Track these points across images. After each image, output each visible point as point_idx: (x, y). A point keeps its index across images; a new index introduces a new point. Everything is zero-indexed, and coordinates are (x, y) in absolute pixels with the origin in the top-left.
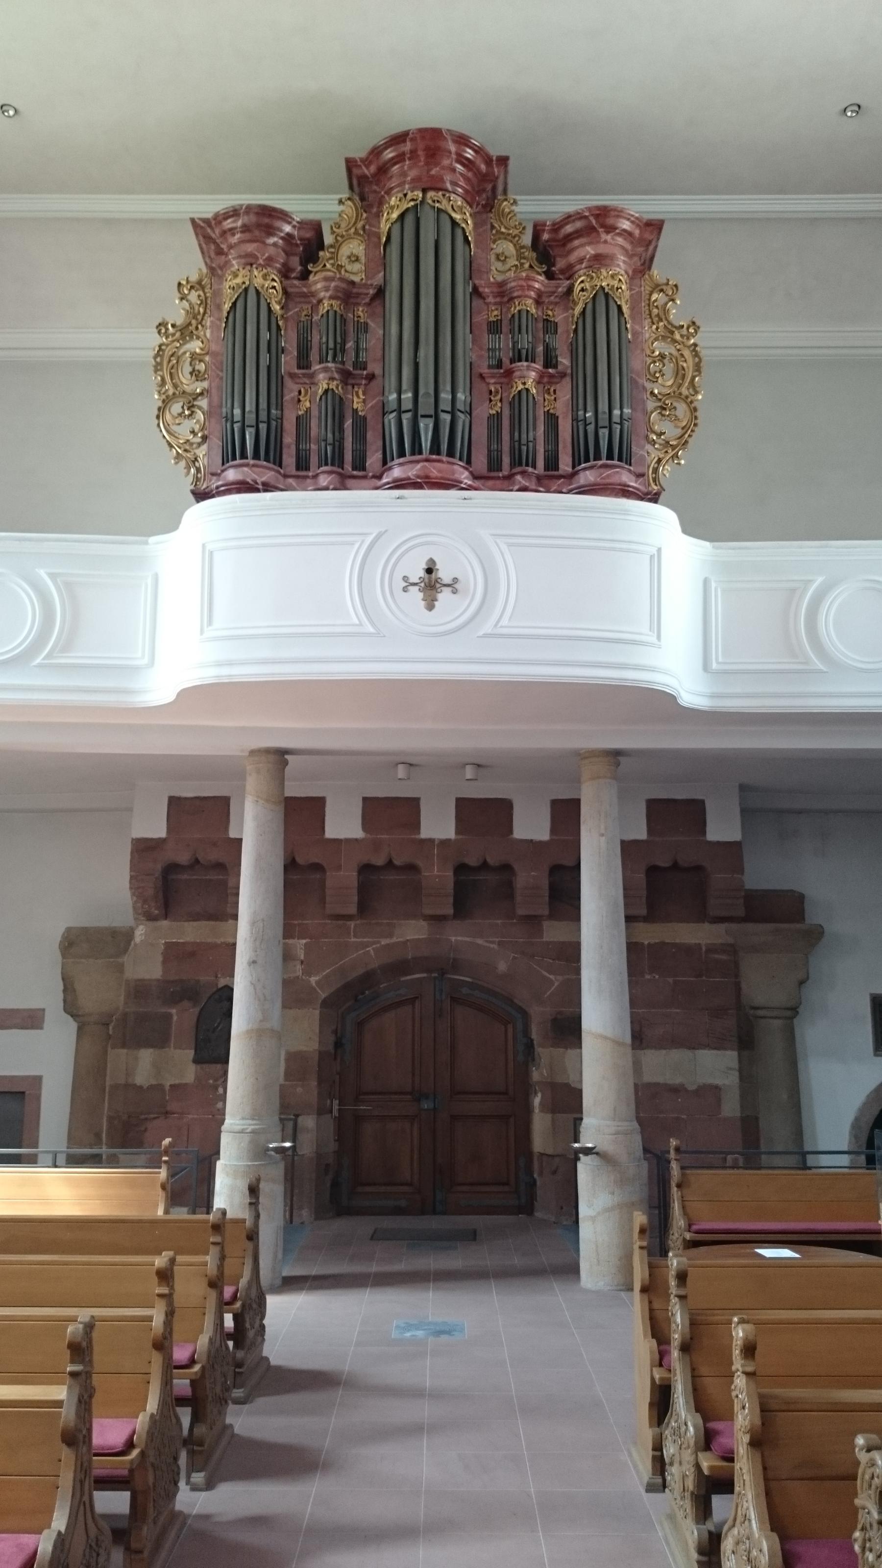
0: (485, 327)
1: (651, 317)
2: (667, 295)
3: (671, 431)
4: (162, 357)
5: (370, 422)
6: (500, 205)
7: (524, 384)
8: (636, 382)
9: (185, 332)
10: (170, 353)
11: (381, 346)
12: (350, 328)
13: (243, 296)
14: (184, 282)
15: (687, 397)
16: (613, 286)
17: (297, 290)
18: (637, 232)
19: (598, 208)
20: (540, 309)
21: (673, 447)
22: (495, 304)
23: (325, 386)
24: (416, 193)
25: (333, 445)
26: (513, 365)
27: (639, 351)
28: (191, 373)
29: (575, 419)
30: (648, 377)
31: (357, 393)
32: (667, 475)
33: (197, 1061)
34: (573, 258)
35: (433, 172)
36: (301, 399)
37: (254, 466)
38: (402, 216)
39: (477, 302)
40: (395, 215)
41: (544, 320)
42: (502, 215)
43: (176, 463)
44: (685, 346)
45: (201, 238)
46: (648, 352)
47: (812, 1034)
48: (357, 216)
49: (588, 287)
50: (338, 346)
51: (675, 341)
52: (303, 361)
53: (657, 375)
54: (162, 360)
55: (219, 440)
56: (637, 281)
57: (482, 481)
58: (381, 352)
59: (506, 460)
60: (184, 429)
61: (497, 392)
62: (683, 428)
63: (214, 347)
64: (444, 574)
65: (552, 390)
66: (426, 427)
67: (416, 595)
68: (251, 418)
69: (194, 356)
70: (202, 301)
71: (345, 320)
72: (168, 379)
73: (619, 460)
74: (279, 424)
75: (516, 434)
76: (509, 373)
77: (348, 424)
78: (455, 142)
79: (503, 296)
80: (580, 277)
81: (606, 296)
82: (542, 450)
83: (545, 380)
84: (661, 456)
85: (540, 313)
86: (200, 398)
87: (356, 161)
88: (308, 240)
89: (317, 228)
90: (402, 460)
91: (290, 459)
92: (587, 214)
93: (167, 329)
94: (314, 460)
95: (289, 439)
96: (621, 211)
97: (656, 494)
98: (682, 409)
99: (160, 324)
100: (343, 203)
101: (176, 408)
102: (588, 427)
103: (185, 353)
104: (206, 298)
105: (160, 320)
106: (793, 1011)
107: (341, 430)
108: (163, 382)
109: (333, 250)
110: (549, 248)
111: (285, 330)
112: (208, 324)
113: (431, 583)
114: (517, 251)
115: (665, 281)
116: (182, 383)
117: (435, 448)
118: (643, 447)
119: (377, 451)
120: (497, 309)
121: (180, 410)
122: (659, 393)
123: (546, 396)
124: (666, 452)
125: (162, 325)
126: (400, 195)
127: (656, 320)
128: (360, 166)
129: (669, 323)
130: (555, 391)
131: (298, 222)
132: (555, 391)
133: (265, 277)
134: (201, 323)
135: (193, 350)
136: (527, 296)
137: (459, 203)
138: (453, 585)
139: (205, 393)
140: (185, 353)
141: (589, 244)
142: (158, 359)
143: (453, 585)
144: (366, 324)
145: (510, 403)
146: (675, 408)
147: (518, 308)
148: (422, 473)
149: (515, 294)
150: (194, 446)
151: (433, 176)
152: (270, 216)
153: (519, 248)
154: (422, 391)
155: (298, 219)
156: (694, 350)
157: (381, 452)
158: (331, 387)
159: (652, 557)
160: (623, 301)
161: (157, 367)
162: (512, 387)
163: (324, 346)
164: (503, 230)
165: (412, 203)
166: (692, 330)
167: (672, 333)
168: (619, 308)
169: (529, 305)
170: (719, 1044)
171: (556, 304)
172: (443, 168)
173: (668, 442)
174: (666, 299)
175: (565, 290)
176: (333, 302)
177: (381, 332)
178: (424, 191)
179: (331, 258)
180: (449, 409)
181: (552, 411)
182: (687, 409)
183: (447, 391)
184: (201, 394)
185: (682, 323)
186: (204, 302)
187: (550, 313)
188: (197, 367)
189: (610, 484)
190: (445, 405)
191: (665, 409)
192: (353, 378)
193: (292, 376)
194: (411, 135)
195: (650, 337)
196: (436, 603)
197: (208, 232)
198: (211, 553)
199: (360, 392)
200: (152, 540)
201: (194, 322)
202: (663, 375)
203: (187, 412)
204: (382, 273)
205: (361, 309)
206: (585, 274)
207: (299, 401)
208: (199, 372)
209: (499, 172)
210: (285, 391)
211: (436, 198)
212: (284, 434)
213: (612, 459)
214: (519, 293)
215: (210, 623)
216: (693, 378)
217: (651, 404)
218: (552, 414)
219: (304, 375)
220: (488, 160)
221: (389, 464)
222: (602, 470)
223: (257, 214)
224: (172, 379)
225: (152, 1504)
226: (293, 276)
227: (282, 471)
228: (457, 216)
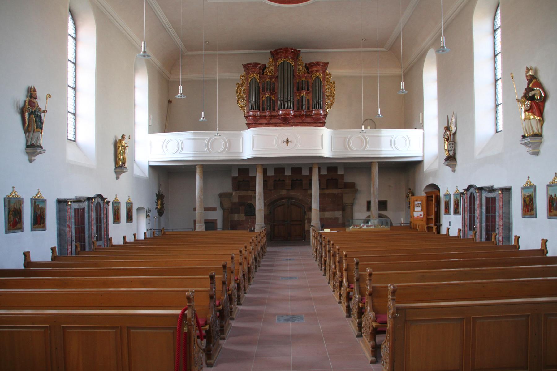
33: (246, 216)
34: (313, 69)
47: (356, 208)
52: (263, 91)
64: (289, 140)
69: (244, 90)
91: (261, 109)
95: (261, 105)
98: (331, 98)
101: (241, 100)
106: (352, 205)
110: (309, 67)
113: (287, 141)
117: (287, 107)
125: (237, 84)
153: (302, 67)
161: (237, 92)
170: (338, 210)
190: (289, 99)
225: (362, 72)
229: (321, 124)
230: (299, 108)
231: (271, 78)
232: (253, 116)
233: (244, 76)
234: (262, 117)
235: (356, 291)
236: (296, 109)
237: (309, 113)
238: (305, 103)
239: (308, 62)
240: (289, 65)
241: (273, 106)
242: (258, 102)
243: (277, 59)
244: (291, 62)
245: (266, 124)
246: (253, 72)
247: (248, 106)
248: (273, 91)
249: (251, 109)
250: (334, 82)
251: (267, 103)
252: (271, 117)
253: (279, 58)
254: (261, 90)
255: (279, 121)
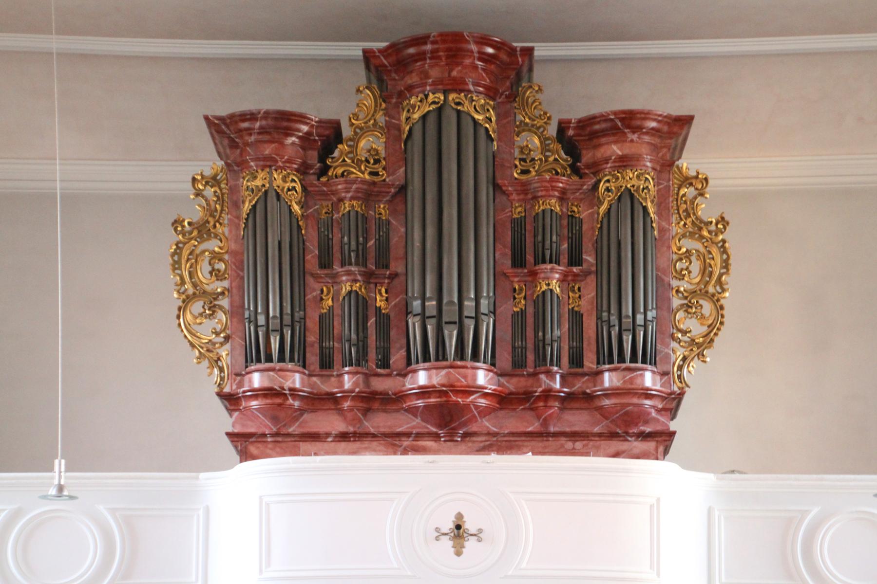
1: (678, 213)
3: (697, 329)
4: (180, 255)
7: (548, 285)
8: (663, 280)
9: (203, 230)
10: (188, 252)
11: (404, 243)
12: (373, 227)
14: (199, 178)
16: (639, 187)
18: (665, 128)
19: (623, 112)
20: (565, 205)
21: (699, 345)
22: (519, 200)
23: (349, 288)
24: (436, 95)
26: (537, 268)
29: (599, 318)
31: (380, 291)
34: (601, 153)
35: (454, 73)
42: (525, 104)
43: (199, 363)
44: (713, 243)
46: (675, 249)
48: (376, 106)
50: (360, 247)
51: (702, 237)
52: (325, 262)
53: (683, 273)
55: (241, 338)
56: (665, 175)
57: (507, 378)
58: (404, 250)
59: (531, 357)
60: (207, 330)
62: (709, 327)
64: (470, 525)
65: (576, 287)
67: (447, 544)
68: (274, 324)
70: (218, 197)
75: (540, 334)
77: (372, 321)
79: (526, 194)
80: (606, 175)
81: (630, 196)
82: (567, 347)
83: (570, 278)
84: (686, 353)
85: (564, 210)
87: (374, 52)
88: (328, 137)
90: (427, 365)
91: (313, 358)
92: (612, 117)
93: (183, 226)
94: (337, 358)
95: (312, 338)
97: (679, 394)
99: (176, 221)
100: (361, 92)
103: (204, 252)
104: (223, 194)
105: (176, 217)
107: (365, 328)
108: (183, 282)
111: (306, 229)
112: (226, 222)
114: (541, 143)
115: (694, 174)
116: (201, 282)
118: (668, 346)
120: (521, 206)
123: (571, 294)
125: (177, 222)
127: (683, 215)
128: (379, 57)
130: (579, 289)
132: (579, 289)
133: (284, 180)
136: (550, 196)
138: (477, 535)
140: (204, 252)
141: (615, 142)
142: (176, 258)
143: (477, 535)
144: (388, 222)
145: (534, 301)
146: (701, 306)
147: (542, 208)
148: (444, 381)
149: (540, 194)
150: (217, 346)
152: (289, 120)
153: (543, 140)
156: (723, 246)
157: (405, 349)
158: (354, 289)
159: (651, 506)
160: (649, 201)
162: (536, 286)
163: (346, 247)
164: (527, 120)
165: (434, 106)
166: (720, 226)
167: (700, 229)
168: (645, 209)
169: (554, 204)
171: (581, 200)
172: (465, 67)
173: (694, 340)
174: (696, 192)
175: (590, 187)
176: (354, 203)
177: (403, 230)
178: (446, 93)
179: (349, 153)
180: (473, 315)
181: (576, 309)
184: (223, 293)
185: (710, 220)
186: (220, 199)
187: (575, 209)
188: (217, 266)
189: (633, 389)
191: (691, 307)
192: (376, 278)
193: (316, 277)
194: (431, 39)
195: (677, 234)
196: (464, 550)
198: (268, 504)
199: (383, 290)
200: (202, 475)
201: (211, 219)
203: (207, 312)
204: (403, 169)
205: (382, 206)
207: (322, 299)
208: (219, 271)
209: (523, 61)
210: (308, 290)
212: (307, 334)
213: (636, 362)
214: (543, 193)
215: (269, 564)
216: (721, 275)
217: (676, 302)
219: (327, 275)
221: (414, 366)
222: (625, 373)
223: (276, 119)
227: (307, 372)
228: (479, 117)
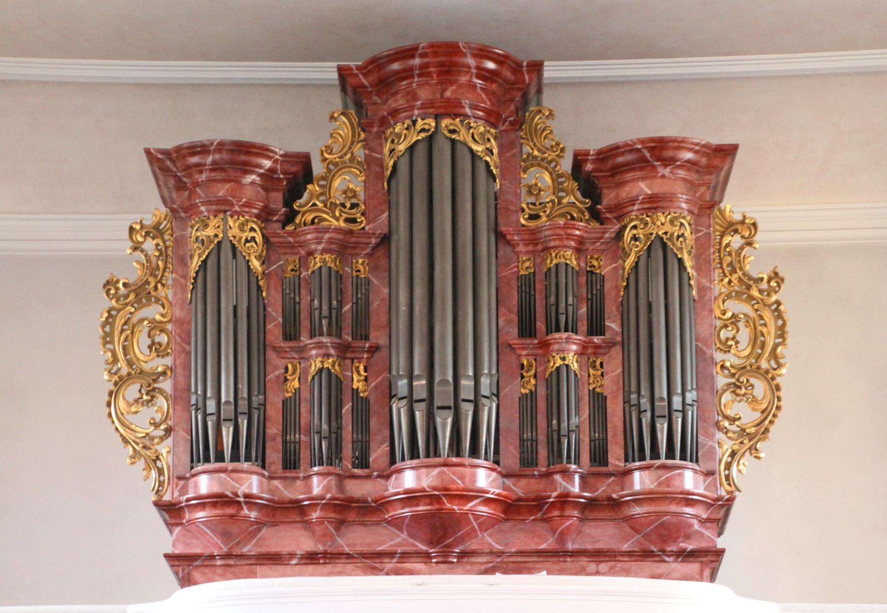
0: (514, 284)
1: (722, 267)
2: (743, 237)
3: (748, 415)
4: (112, 325)
5: (374, 408)
6: (533, 119)
7: (563, 359)
8: (704, 353)
9: (141, 293)
10: (123, 321)
11: (387, 308)
13: (215, 252)
14: (138, 227)
15: (767, 372)
17: (281, 240)
20: (583, 259)
21: (751, 437)
22: (527, 252)
23: (319, 365)
24: (426, 121)
25: (329, 438)
26: (549, 337)
27: (706, 313)
28: (150, 347)
29: (627, 401)
30: (718, 345)
32: (744, 472)
35: (448, 94)
36: (289, 377)
37: (233, 471)
38: (411, 149)
39: (505, 250)
40: (402, 147)
41: (588, 272)
42: (534, 132)
45: (158, 171)
46: (718, 313)
48: (353, 136)
49: (641, 236)
51: (751, 298)
52: (290, 333)
54: (112, 330)
55: (187, 433)
56: (704, 220)
57: (513, 480)
59: (543, 452)
60: (143, 420)
61: (530, 366)
62: (763, 412)
63: (178, 313)
65: (598, 363)
66: (445, 425)
68: (227, 411)
69: (156, 326)
70: (161, 254)
71: (341, 276)
72: (121, 355)
73: (681, 459)
74: (262, 411)
75: (555, 422)
76: (545, 345)
77: (347, 408)
78: (475, 56)
79: (536, 244)
80: (632, 220)
82: (587, 440)
83: (590, 351)
84: (736, 447)
86: (161, 378)
89: (304, 161)
90: (415, 462)
91: (274, 456)
92: (639, 146)
93: (117, 289)
94: (305, 455)
95: (274, 429)
96: (682, 142)
98: (760, 388)
99: (108, 282)
101: (132, 391)
102: (642, 415)
103: (142, 321)
104: (166, 248)
107: (339, 416)
108: (115, 360)
109: (324, 183)
110: (597, 177)
111: (267, 290)
112: (170, 282)
114: (553, 180)
116: (138, 359)
117: (456, 447)
118: (712, 437)
119: (382, 443)
120: (529, 260)
121: (138, 395)
122: (731, 366)
123: (591, 371)
124: (742, 443)
125: (109, 284)
126: (408, 122)
127: (727, 270)
128: (356, 75)
129: (745, 274)
130: (601, 365)
131: (281, 156)
132: (601, 365)
133: (242, 228)
134: (160, 281)
135: (151, 317)
137: (482, 129)
139: (169, 372)
140: (142, 321)
141: (643, 179)
142: (107, 329)
144: (368, 282)
145: (547, 380)
147: (554, 262)
149: (552, 244)
150: (156, 441)
151: (448, 100)
152: (248, 153)
153: (556, 177)
154: (437, 378)
155: (282, 152)
156: (777, 310)
157: (387, 444)
158: (326, 366)
160: (685, 251)
161: (107, 338)
162: (549, 361)
163: (317, 312)
164: (536, 153)
165: (423, 135)
166: (773, 284)
168: (680, 261)
171: (603, 251)
172: (460, 86)
173: (743, 430)
175: (613, 235)
176: (327, 257)
177: (386, 291)
178: (437, 117)
179: (321, 194)
180: (472, 398)
181: (598, 390)
182: (768, 387)
183: (468, 377)
184: (164, 373)
186: (163, 254)
187: (595, 263)
188: (157, 339)
191: (740, 387)
192: (352, 352)
193: (277, 350)
195: (721, 294)
197: (174, 168)
199: (362, 368)
201: (151, 279)
202: (737, 343)
203: (145, 397)
204: (386, 215)
205: (360, 261)
206: (637, 218)
207: (286, 380)
208: (160, 344)
209: (530, 79)
210: (269, 369)
211: (452, 127)
212: (268, 424)
213: (674, 458)
214: (557, 243)
217: (721, 381)
218: (598, 394)
220: (517, 67)
221: (399, 465)
222: (660, 472)
224: (125, 354)
226: (275, 218)
227: (266, 473)
228: (478, 148)
229: (693, 567)
230: (536, 448)
231: (345, 246)
232: (218, 500)
233: (155, 231)
234: (283, 511)
235: (429, 507)
236: (511, 456)
237: (603, 488)
238: (578, 419)
239: (595, 143)
240: (465, 164)
241: (353, 433)
242: (256, 413)
243: (384, 123)
244: (478, 137)
245: (311, 558)
246: (222, 207)
247: (182, 435)
248: (355, 335)
249: (204, 452)
250: (775, 275)
251: (314, 415)
252: (346, 510)
253: (394, 113)
254: (274, 328)
255: (398, 540)
